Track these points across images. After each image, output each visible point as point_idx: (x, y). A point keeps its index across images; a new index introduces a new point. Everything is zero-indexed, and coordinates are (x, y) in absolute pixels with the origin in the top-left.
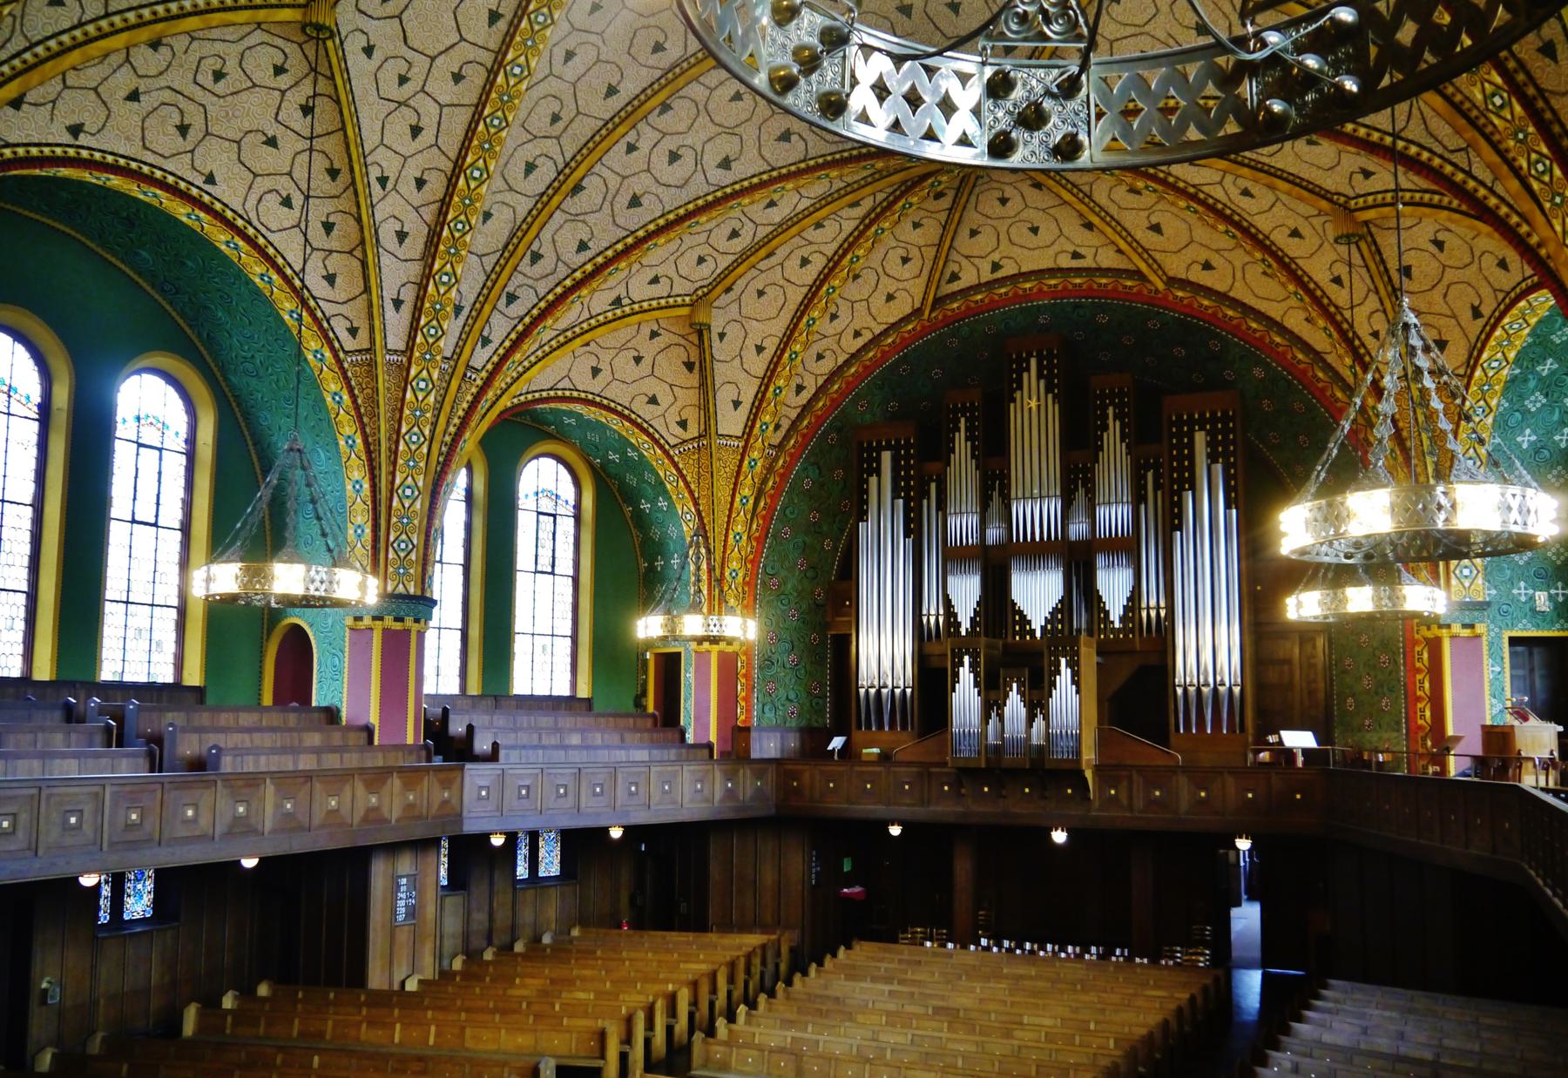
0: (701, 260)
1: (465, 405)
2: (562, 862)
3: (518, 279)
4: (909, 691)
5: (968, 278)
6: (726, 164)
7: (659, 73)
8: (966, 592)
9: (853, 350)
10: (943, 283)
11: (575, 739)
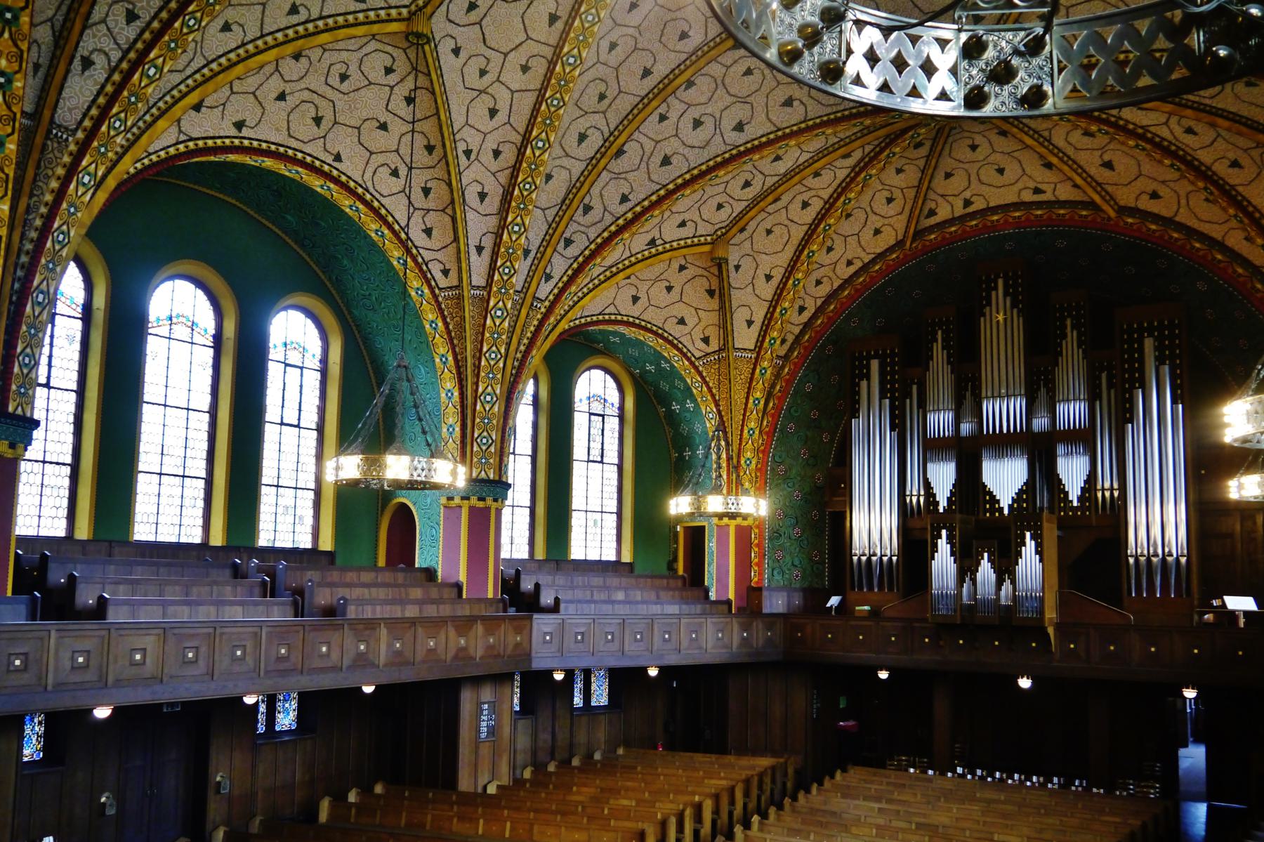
0: (720, 206)
1: (532, 329)
2: (609, 695)
3: (573, 227)
4: (895, 559)
5: (944, 213)
7: (685, 56)
8: (943, 476)
9: (846, 277)
10: (922, 218)
11: (620, 596)
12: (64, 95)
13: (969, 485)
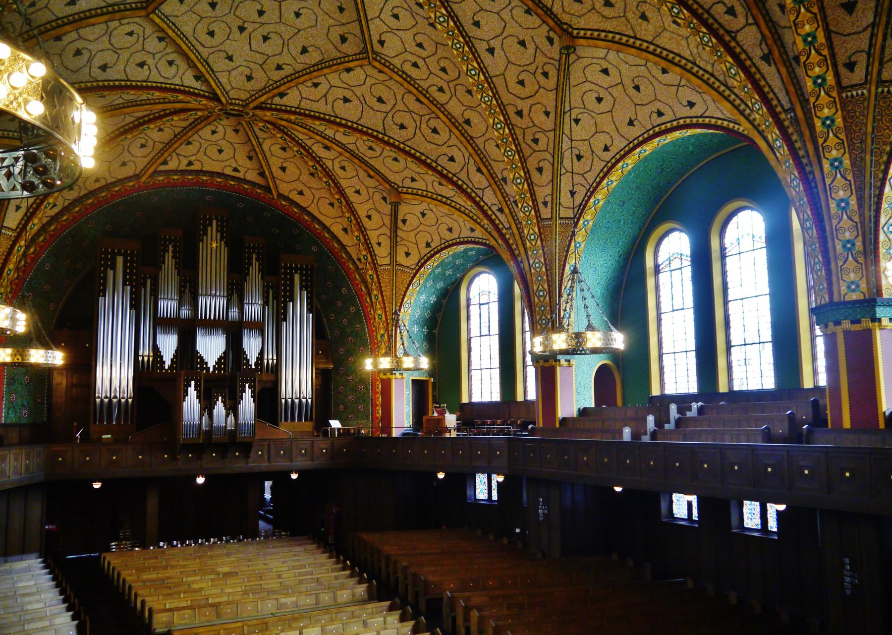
4: (130, 400)
5: (172, 165)
6: (104, 68)
8: (168, 344)
12: (784, 91)
13: (187, 350)
